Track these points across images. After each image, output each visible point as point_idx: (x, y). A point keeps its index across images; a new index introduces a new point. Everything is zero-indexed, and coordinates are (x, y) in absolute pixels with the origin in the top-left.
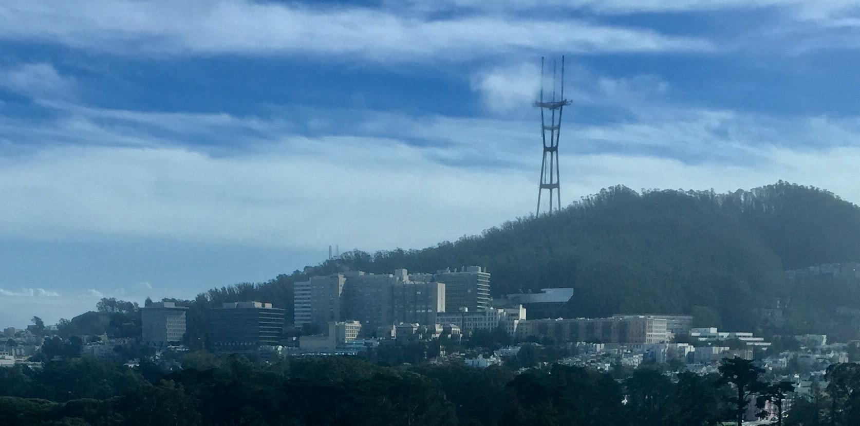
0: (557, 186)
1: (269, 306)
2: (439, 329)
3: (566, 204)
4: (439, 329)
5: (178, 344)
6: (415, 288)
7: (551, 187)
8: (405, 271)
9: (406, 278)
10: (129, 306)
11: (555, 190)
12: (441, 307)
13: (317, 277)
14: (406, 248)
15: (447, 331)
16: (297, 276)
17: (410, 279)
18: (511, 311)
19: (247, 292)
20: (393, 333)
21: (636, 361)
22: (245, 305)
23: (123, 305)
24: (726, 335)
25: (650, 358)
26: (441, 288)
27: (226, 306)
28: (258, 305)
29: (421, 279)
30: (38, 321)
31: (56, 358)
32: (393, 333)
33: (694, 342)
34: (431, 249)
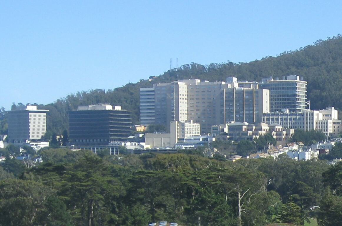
1: (118, 108)
2: (265, 127)
4: (265, 127)
5: (40, 140)
8: (235, 79)
9: (236, 85)
12: (266, 108)
13: (160, 84)
15: (272, 129)
16: (143, 83)
17: (240, 86)
18: (324, 112)
19: (98, 97)
20: (226, 130)
22: (98, 107)
26: (266, 94)
27: (81, 108)
28: (109, 107)
29: (253, 86)
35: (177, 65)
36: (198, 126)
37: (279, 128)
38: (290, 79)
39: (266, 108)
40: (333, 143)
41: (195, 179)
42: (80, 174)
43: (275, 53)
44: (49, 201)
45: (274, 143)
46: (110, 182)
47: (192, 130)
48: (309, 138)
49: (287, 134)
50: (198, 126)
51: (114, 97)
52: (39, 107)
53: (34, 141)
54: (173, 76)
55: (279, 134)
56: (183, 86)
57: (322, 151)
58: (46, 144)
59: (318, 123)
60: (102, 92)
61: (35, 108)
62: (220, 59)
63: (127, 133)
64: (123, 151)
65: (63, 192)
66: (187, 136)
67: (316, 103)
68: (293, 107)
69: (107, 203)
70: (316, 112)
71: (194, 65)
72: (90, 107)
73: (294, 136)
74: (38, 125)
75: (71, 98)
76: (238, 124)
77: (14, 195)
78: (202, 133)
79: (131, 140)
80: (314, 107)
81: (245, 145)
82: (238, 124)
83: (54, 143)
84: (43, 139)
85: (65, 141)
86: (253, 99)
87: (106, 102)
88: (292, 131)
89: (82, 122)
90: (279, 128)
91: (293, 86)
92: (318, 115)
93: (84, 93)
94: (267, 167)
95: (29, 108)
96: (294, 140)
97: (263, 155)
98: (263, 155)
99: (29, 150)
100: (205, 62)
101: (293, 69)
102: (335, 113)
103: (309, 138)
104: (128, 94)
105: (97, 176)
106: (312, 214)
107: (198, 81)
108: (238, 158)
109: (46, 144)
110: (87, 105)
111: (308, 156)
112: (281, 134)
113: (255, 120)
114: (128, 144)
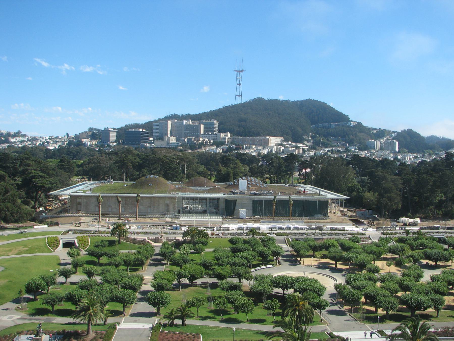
0: (241, 84)
1: (144, 130)
2: (201, 139)
3: (244, 101)
4: (201, 139)
5: (113, 142)
6: (194, 126)
7: (239, 96)
8: (190, 120)
9: (191, 123)
10: (98, 130)
11: (240, 97)
12: (202, 132)
13: (161, 122)
14: (191, 114)
15: (204, 140)
16: (155, 121)
17: (192, 123)
18: (225, 134)
19: (137, 126)
20: (186, 140)
21: (265, 152)
22: (136, 130)
23: (96, 130)
24: (294, 144)
25: (270, 153)
26: (202, 126)
27: (130, 130)
28: (141, 130)
29: (197, 123)
30: (67, 134)
31: (72, 146)
32: (186, 140)
33: (284, 146)
34: (220, 109)
35: (169, 114)
36: (175, 138)
37: (207, 140)
38: (212, 121)
39: (202, 132)
40: (228, 146)
41: (168, 159)
42: (123, 155)
43: (207, 111)
44: (111, 166)
45: (205, 146)
46: (135, 159)
47: (173, 140)
48: (218, 144)
49: (210, 142)
50: (175, 138)
51: (143, 126)
52: (114, 129)
53: (111, 142)
54: (167, 118)
55: (207, 142)
56: (170, 123)
57: (223, 149)
58: (115, 144)
59: (222, 138)
60: (139, 124)
61: (112, 130)
62: (185, 113)
63: (147, 141)
64: (146, 147)
65: (116, 162)
66: (171, 142)
67: (222, 130)
68: (213, 132)
69: (134, 167)
70: (221, 134)
71: (175, 115)
72: (133, 130)
73: (213, 143)
74: (113, 136)
75: (126, 126)
76: (191, 138)
77: (208, 161)
78: (177, 141)
79: (149, 143)
80: (221, 132)
81: (193, 146)
82: (191, 138)
83: (119, 144)
84: (116, 142)
85: (123, 142)
86: (198, 128)
87: (140, 128)
88: (212, 141)
89: (128, 134)
90: (207, 140)
91: (213, 124)
92: (222, 135)
93: (131, 124)
94: (200, 156)
95: (110, 129)
96: (212, 145)
97: (200, 150)
98: (200, 150)
99: (109, 146)
100: (180, 114)
101: (214, 117)
102: (229, 135)
103: (218, 144)
104: (149, 126)
105: (130, 157)
106: (374, 263)
107: (176, 121)
108: (190, 151)
109: (115, 144)
110: (132, 129)
111: (218, 151)
112: (207, 142)
113: (198, 136)
114: (148, 144)
